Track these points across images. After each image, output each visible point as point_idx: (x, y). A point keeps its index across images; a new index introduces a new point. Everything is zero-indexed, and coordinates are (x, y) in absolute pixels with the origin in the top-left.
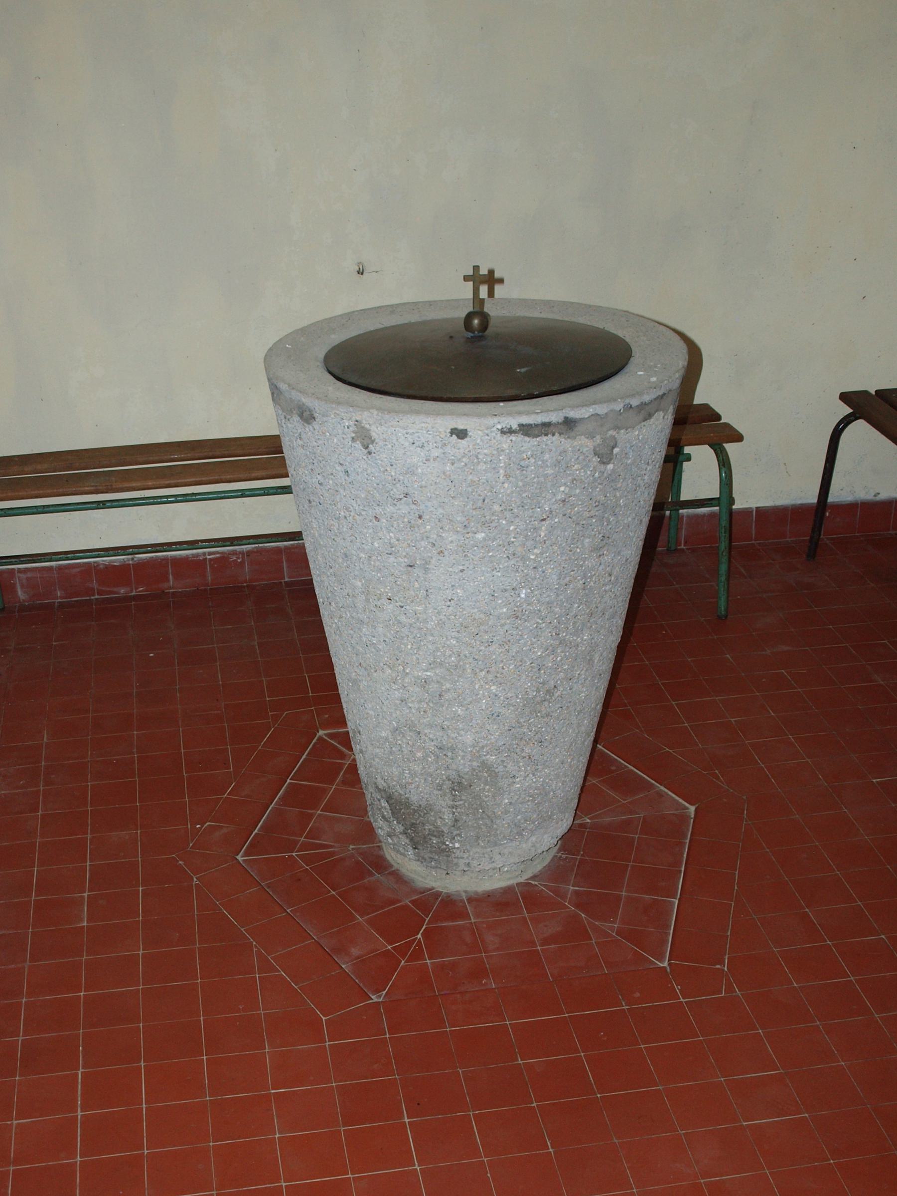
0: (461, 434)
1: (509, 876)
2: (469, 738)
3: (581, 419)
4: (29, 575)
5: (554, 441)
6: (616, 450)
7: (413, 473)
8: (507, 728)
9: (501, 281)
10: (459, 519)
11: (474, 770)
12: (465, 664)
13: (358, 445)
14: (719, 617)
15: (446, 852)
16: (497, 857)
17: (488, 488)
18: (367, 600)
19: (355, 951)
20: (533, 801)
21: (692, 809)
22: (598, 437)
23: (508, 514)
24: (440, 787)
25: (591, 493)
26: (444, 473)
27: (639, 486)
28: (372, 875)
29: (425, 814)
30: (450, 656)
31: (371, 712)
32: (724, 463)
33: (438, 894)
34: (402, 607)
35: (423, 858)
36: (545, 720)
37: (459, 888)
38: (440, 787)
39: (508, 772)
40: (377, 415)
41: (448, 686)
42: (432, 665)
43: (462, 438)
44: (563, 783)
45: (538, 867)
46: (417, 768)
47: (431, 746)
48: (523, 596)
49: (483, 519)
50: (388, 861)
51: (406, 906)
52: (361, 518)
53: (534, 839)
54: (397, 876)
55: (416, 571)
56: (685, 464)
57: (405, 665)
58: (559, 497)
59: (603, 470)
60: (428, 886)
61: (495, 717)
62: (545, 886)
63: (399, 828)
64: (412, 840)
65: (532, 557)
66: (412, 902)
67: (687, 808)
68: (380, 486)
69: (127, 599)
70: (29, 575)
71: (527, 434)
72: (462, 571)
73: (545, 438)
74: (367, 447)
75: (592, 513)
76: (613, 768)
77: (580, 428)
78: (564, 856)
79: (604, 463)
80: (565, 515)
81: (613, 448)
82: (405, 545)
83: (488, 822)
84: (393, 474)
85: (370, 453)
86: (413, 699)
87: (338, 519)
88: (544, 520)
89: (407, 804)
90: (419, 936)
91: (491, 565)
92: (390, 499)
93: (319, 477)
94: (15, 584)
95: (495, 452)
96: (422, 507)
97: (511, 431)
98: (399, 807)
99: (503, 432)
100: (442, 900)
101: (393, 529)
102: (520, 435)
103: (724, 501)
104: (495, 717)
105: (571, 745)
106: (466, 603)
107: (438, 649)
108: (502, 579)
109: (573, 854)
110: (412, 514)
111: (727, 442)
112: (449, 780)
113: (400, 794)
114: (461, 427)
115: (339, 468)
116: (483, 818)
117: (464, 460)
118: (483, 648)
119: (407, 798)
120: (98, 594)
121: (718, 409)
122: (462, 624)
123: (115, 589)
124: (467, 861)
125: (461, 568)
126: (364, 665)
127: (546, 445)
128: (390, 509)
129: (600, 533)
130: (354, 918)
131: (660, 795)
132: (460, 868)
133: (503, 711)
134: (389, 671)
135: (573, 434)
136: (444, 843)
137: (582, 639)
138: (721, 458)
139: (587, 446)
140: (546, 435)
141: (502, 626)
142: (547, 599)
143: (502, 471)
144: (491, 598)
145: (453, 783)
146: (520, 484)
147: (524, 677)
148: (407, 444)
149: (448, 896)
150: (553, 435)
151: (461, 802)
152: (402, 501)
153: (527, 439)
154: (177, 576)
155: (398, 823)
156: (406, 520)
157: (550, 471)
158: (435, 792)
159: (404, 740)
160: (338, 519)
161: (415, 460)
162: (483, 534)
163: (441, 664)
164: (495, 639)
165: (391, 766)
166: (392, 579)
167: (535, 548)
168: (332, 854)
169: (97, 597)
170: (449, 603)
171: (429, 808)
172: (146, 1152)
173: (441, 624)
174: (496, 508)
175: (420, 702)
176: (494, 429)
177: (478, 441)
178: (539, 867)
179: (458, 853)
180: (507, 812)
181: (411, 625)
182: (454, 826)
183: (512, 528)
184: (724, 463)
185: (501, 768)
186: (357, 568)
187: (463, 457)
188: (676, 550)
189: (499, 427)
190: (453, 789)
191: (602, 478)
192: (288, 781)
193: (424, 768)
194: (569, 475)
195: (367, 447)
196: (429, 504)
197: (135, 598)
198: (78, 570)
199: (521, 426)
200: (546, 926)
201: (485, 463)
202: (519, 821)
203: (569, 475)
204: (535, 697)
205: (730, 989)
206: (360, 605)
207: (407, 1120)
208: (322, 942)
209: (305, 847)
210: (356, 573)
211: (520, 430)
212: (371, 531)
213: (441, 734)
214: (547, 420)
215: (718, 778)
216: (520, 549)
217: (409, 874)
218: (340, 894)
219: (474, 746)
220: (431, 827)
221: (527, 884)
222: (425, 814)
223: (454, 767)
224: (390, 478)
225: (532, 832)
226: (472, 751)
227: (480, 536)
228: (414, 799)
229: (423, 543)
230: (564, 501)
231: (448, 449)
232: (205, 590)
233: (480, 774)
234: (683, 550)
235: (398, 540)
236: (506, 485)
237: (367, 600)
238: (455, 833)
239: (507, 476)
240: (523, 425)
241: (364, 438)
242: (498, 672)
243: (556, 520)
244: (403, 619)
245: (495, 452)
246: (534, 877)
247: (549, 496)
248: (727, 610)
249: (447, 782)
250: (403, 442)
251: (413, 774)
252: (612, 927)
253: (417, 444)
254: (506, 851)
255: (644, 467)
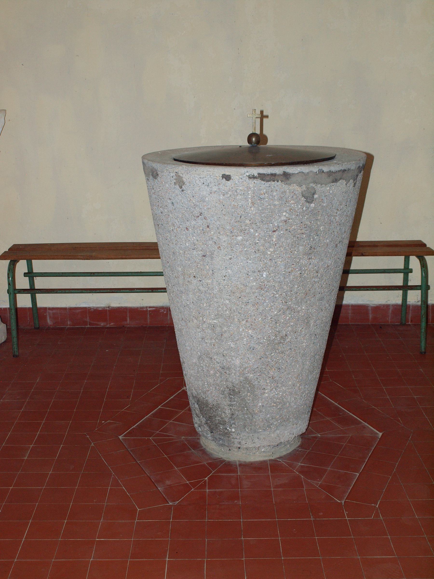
0: (227, 178)
1: (264, 454)
2: (237, 362)
3: (293, 174)
4: (54, 311)
5: (278, 185)
6: (316, 196)
7: (204, 201)
8: (258, 357)
9: (267, 117)
10: (228, 228)
11: (241, 382)
12: (234, 316)
13: (177, 187)
14: (421, 353)
15: (227, 434)
16: (256, 440)
17: (243, 210)
18: (184, 278)
19: (168, 482)
20: (275, 406)
21: (380, 434)
22: (304, 186)
23: (254, 226)
24: (223, 392)
25: (302, 219)
26: (219, 200)
27: (333, 222)
28: (190, 449)
29: (216, 410)
30: (226, 310)
31: (188, 348)
32: (424, 266)
33: (224, 461)
34: (200, 281)
35: (216, 438)
36: (281, 355)
37: (236, 459)
38: (223, 392)
39: (260, 385)
40: (186, 168)
41: (225, 329)
42: (218, 316)
43: (228, 180)
44: (295, 399)
45: (284, 452)
46: (211, 381)
47: (218, 366)
48: (264, 276)
49: (241, 228)
50: (201, 445)
51: (204, 465)
52: (180, 229)
53: (278, 432)
54: (204, 452)
55: (207, 259)
56: (410, 274)
57: (203, 316)
58: (283, 218)
59: (308, 206)
60: (220, 457)
61: (252, 349)
62: (285, 462)
63: (204, 420)
64: (210, 427)
65: (269, 253)
66: (208, 464)
67: (378, 434)
68: (188, 210)
69: (104, 328)
70: (54, 311)
71: (262, 180)
72: (230, 259)
73: (273, 183)
74: (181, 187)
75: (303, 231)
76: (341, 414)
77: (293, 179)
78: (300, 450)
79: (308, 202)
80: (287, 230)
81: (314, 194)
82: (201, 243)
83: (250, 416)
84: (194, 202)
85: (183, 191)
86: (208, 337)
87: (170, 232)
88: (274, 231)
89: (207, 404)
90: (206, 478)
91: (246, 256)
92: (193, 217)
93: (161, 209)
94: (46, 316)
95: (246, 189)
96: (209, 221)
97: (254, 177)
98: (203, 405)
99: (250, 177)
100: (225, 464)
101: (195, 235)
102: (259, 180)
103: (424, 287)
104: (252, 349)
105: (299, 375)
106: (233, 278)
107: (219, 306)
108: (252, 264)
109: (306, 449)
110: (204, 225)
111: (426, 255)
112: (228, 388)
113: (203, 398)
114: (227, 174)
115: (169, 201)
116: (247, 414)
117: (229, 193)
118: (243, 306)
119: (207, 400)
120: (89, 325)
121: (425, 242)
122: (231, 291)
123: (99, 323)
124: (239, 441)
125: (230, 257)
126: (184, 319)
127: (274, 187)
128: (193, 223)
129: (308, 244)
130: (172, 467)
131: (364, 427)
132: (235, 445)
133: (257, 346)
134: (195, 321)
135: (289, 182)
136: (226, 429)
137: (301, 308)
138: (422, 263)
139: (298, 191)
140: (274, 181)
141: (253, 293)
142: (279, 280)
143: (250, 200)
144: (247, 276)
145: (230, 390)
146: (260, 208)
147: (267, 326)
148: (200, 184)
149: (229, 462)
150: (278, 181)
151: (235, 403)
152: (199, 218)
153: (263, 182)
154: (131, 319)
155: (203, 417)
156: (201, 229)
157: (277, 203)
158: (221, 396)
159: (204, 363)
160: (170, 232)
161: (205, 193)
162: (241, 237)
163: (221, 315)
164: (250, 301)
165: (199, 380)
166: (195, 264)
167: (270, 248)
168: (173, 439)
169: (88, 326)
170: (224, 278)
171: (218, 406)
172: (16, 560)
173: (221, 291)
174: (247, 222)
175: (211, 339)
176: (245, 175)
177: (237, 182)
178: (285, 453)
179: (234, 435)
180: (261, 411)
181: (205, 291)
182: (231, 418)
183: (257, 234)
184: (424, 266)
185: (256, 383)
186: (179, 260)
187: (229, 191)
188: (405, 324)
189: (248, 174)
190: (230, 394)
191: (308, 211)
192: (159, 407)
193: (214, 381)
194: (288, 206)
195: (181, 187)
196: (212, 219)
197: (108, 328)
198: (80, 311)
199: (259, 174)
200: (279, 480)
201: (240, 195)
202: (269, 418)
203: (288, 206)
204: (274, 339)
205: (377, 515)
206: (181, 282)
207: (167, 559)
208: (151, 477)
209: (158, 435)
210: (179, 263)
211: (259, 177)
212: (185, 236)
213: (222, 359)
214: (274, 172)
215: (399, 421)
216: (262, 248)
217: (211, 451)
218: (169, 457)
219: (240, 367)
220: (219, 418)
221: (275, 460)
222: (216, 410)
223: (231, 380)
224: (193, 204)
225: (277, 427)
226: (239, 370)
227: (240, 238)
228: (210, 400)
229: (210, 242)
230: (286, 221)
231: (221, 187)
232: (146, 327)
233: (244, 385)
234: (409, 325)
235: (197, 241)
236: (252, 209)
237: (184, 278)
238: (232, 422)
239: (253, 203)
240: (260, 174)
241: (180, 182)
242: (252, 322)
243: (282, 232)
244: (201, 288)
245: (246, 189)
246: (280, 458)
247: (277, 217)
248: (425, 348)
249: (227, 389)
250: (198, 183)
251: (209, 385)
252: (317, 483)
253: (205, 183)
254: (262, 437)
255: (336, 211)
